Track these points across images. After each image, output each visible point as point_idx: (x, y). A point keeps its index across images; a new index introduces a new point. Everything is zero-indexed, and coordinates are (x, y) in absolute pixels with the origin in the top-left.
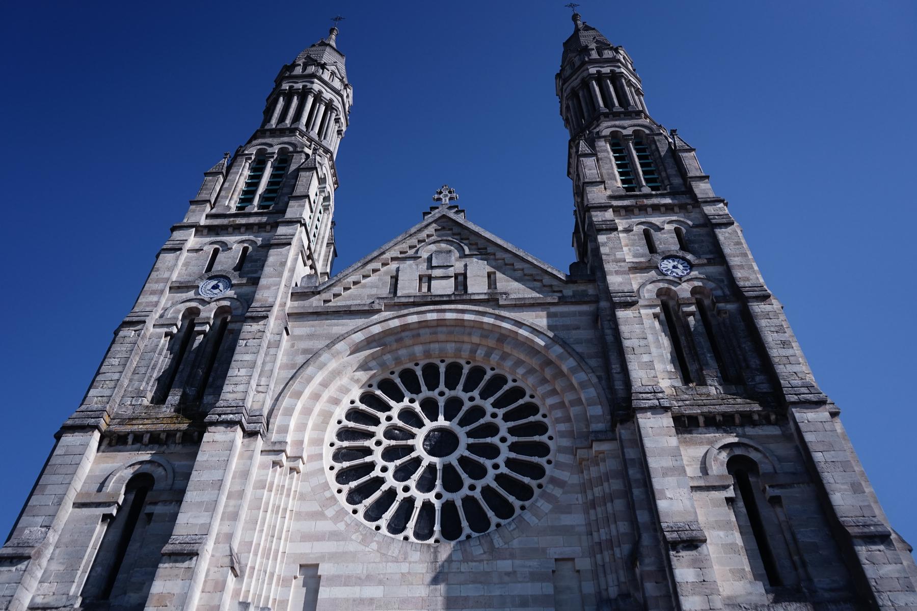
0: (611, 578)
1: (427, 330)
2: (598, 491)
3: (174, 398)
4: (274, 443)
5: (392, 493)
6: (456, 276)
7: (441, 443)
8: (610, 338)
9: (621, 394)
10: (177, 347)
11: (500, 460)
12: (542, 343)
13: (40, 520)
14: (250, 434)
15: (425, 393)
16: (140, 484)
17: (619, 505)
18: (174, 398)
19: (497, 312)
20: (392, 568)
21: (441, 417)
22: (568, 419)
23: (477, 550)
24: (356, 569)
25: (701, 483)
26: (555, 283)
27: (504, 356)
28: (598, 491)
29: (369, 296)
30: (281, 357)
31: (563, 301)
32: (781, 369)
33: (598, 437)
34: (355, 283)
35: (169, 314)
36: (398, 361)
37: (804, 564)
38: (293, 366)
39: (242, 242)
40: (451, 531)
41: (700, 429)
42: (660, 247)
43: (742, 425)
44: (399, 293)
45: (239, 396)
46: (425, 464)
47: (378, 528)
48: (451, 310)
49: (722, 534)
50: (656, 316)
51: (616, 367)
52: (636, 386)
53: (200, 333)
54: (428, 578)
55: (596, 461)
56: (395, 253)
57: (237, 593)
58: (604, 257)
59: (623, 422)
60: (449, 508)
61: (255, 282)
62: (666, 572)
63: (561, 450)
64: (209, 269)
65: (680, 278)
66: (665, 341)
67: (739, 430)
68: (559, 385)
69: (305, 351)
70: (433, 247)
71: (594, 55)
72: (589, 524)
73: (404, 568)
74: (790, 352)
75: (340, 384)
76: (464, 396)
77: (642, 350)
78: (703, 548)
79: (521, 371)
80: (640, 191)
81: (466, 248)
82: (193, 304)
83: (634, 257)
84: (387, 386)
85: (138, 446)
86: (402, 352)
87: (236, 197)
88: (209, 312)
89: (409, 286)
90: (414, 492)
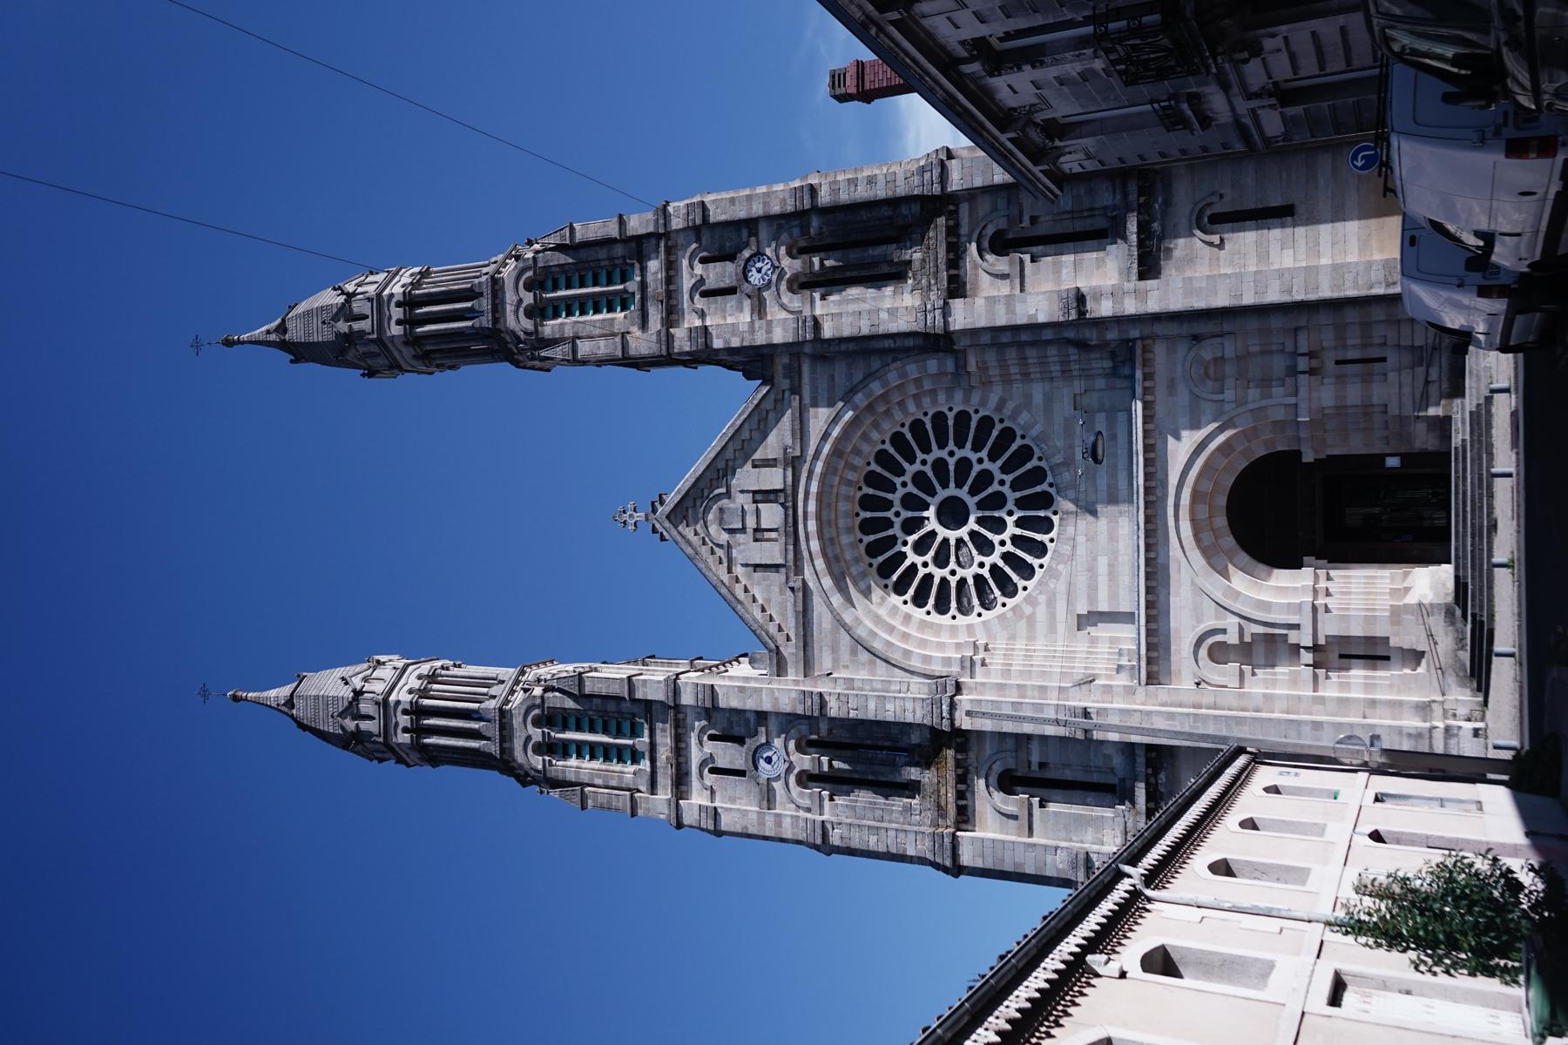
0: (1095, 364)
1: (825, 531)
2: (1014, 370)
3: (913, 773)
4: (963, 667)
5: (1006, 557)
6: (755, 502)
7: (953, 514)
8: (852, 346)
9: (920, 341)
10: (845, 788)
11: (974, 457)
12: (850, 413)
13: (1049, 858)
14: (958, 688)
15: (896, 530)
16: (1008, 783)
17: (1031, 353)
18: (913, 773)
19: (809, 458)
20: (1081, 551)
21: (925, 514)
22: (933, 393)
23: (1067, 476)
24: (1082, 581)
25: (1018, 281)
26: (772, 396)
27: (857, 452)
28: (1014, 370)
29: (782, 592)
30: (863, 675)
31: (796, 390)
32: (902, 190)
33: (961, 366)
34: (763, 610)
35: (806, 802)
36: (857, 560)
37: (1092, 209)
38: (872, 663)
39: (701, 742)
40: (1046, 501)
41: (962, 273)
42: (727, 282)
43: (958, 236)
44: (781, 561)
45: (918, 705)
46: (976, 528)
47: (1041, 566)
48: (805, 506)
49: (1064, 271)
50: (823, 298)
51: (887, 344)
52: (914, 327)
53: (830, 765)
54: (1090, 518)
55: (983, 368)
56: (722, 572)
57: (1109, 677)
58: (746, 344)
59: (952, 343)
60: (1020, 504)
61: (762, 716)
62: (1101, 323)
63: (967, 400)
64: (741, 773)
65: (775, 268)
66: (854, 291)
67: (963, 239)
68: (896, 398)
69: (854, 653)
70: (713, 529)
71: (365, 325)
72: (1043, 379)
73: (1081, 539)
74: (881, 180)
75: (887, 615)
76: (901, 492)
77: (874, 317)
78: (1084, 290)
79: (876, 436)
80: (633, 294)
81: (717, 491)
82: (792, 779)
83: (741, 311)
84: (885, 571)
85: (968, 795)
86: (848, 555)
87: (616, 767)
88: (804, 762)
89: (772, 552)
90: (1006, 536)
